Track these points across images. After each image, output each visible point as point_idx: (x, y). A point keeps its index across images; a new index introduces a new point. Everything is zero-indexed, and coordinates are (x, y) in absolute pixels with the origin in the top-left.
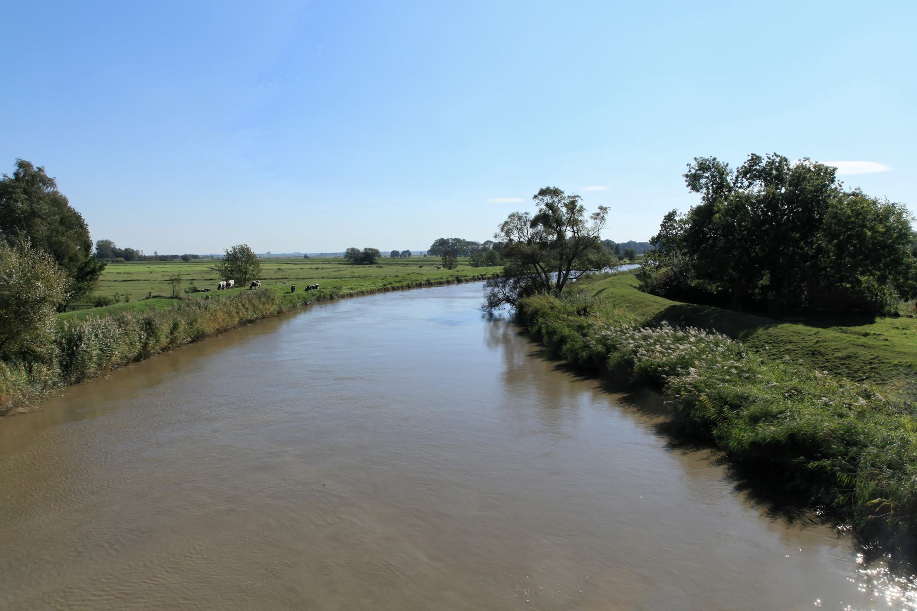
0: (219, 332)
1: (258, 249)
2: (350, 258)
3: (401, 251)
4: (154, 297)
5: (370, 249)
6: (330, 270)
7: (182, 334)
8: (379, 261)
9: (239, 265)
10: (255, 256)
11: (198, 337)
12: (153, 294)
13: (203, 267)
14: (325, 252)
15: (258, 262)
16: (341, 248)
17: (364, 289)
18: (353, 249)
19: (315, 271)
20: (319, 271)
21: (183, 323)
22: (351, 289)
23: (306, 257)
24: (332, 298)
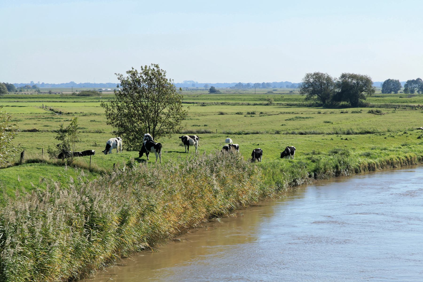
0: (182, 231)
1: (177, 76)
2: (313, 92)
3: (403, 79)
4: (30, 162)
5: (353, 77)
6: (277, 117)
7: (132, 235)
8: (369, 100)
9: (143, 109)
10: (171, 87)
11: (154, 239)
12: (27, 157)
13: (34, 108)
14: (245, 81)
15: (178, 101)
16: (296, 77)
17: (393, 156)
18: (318, 76)
19: (249, 119)
20: (257, 119)
21: (135, 211)
22: (368, 155)
23: (212, 90)
24: (338, 174)
